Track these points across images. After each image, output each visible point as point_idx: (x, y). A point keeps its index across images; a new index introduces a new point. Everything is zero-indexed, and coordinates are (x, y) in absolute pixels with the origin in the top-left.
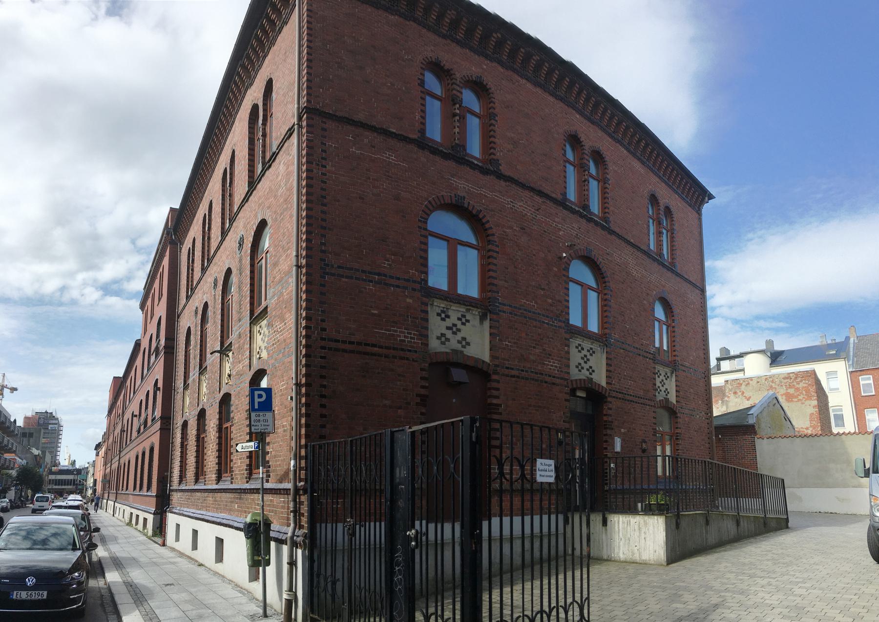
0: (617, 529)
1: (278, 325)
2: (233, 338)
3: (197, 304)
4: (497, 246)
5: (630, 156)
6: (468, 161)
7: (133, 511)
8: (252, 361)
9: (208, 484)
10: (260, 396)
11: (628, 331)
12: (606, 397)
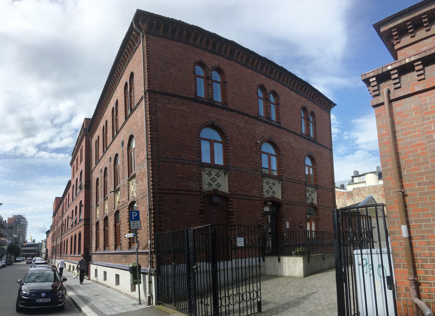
0: (285, 263)
1: (140, 183)
4: (230, 141)
5: (290, 91)
6: (216, 105)
7: (71, 264)
9: (110, 251)
10: (135, 214)
11: (291, 173)
12: (282, 204)
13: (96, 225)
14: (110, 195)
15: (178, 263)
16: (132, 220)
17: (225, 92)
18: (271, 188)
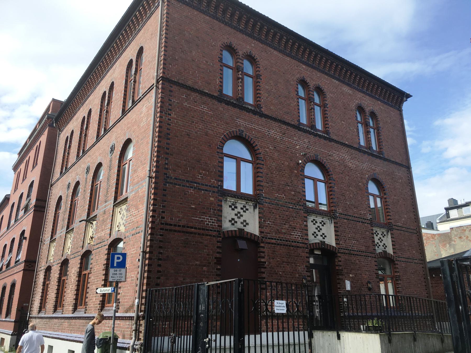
2: (97, 212)
3: (70, 180)
4: (263, 160)
6: (245, 107)
8: (112, 232)
10: (118, 258)
13: (46, 272)
14: (77, 225)
15: (180, 335)
16: (113, 267)
17: (257, 90)
18: (319, 229)
